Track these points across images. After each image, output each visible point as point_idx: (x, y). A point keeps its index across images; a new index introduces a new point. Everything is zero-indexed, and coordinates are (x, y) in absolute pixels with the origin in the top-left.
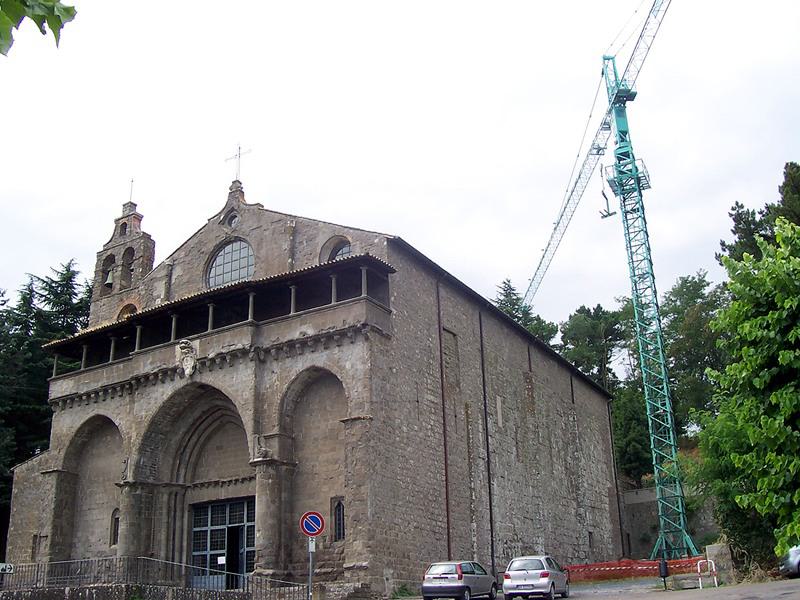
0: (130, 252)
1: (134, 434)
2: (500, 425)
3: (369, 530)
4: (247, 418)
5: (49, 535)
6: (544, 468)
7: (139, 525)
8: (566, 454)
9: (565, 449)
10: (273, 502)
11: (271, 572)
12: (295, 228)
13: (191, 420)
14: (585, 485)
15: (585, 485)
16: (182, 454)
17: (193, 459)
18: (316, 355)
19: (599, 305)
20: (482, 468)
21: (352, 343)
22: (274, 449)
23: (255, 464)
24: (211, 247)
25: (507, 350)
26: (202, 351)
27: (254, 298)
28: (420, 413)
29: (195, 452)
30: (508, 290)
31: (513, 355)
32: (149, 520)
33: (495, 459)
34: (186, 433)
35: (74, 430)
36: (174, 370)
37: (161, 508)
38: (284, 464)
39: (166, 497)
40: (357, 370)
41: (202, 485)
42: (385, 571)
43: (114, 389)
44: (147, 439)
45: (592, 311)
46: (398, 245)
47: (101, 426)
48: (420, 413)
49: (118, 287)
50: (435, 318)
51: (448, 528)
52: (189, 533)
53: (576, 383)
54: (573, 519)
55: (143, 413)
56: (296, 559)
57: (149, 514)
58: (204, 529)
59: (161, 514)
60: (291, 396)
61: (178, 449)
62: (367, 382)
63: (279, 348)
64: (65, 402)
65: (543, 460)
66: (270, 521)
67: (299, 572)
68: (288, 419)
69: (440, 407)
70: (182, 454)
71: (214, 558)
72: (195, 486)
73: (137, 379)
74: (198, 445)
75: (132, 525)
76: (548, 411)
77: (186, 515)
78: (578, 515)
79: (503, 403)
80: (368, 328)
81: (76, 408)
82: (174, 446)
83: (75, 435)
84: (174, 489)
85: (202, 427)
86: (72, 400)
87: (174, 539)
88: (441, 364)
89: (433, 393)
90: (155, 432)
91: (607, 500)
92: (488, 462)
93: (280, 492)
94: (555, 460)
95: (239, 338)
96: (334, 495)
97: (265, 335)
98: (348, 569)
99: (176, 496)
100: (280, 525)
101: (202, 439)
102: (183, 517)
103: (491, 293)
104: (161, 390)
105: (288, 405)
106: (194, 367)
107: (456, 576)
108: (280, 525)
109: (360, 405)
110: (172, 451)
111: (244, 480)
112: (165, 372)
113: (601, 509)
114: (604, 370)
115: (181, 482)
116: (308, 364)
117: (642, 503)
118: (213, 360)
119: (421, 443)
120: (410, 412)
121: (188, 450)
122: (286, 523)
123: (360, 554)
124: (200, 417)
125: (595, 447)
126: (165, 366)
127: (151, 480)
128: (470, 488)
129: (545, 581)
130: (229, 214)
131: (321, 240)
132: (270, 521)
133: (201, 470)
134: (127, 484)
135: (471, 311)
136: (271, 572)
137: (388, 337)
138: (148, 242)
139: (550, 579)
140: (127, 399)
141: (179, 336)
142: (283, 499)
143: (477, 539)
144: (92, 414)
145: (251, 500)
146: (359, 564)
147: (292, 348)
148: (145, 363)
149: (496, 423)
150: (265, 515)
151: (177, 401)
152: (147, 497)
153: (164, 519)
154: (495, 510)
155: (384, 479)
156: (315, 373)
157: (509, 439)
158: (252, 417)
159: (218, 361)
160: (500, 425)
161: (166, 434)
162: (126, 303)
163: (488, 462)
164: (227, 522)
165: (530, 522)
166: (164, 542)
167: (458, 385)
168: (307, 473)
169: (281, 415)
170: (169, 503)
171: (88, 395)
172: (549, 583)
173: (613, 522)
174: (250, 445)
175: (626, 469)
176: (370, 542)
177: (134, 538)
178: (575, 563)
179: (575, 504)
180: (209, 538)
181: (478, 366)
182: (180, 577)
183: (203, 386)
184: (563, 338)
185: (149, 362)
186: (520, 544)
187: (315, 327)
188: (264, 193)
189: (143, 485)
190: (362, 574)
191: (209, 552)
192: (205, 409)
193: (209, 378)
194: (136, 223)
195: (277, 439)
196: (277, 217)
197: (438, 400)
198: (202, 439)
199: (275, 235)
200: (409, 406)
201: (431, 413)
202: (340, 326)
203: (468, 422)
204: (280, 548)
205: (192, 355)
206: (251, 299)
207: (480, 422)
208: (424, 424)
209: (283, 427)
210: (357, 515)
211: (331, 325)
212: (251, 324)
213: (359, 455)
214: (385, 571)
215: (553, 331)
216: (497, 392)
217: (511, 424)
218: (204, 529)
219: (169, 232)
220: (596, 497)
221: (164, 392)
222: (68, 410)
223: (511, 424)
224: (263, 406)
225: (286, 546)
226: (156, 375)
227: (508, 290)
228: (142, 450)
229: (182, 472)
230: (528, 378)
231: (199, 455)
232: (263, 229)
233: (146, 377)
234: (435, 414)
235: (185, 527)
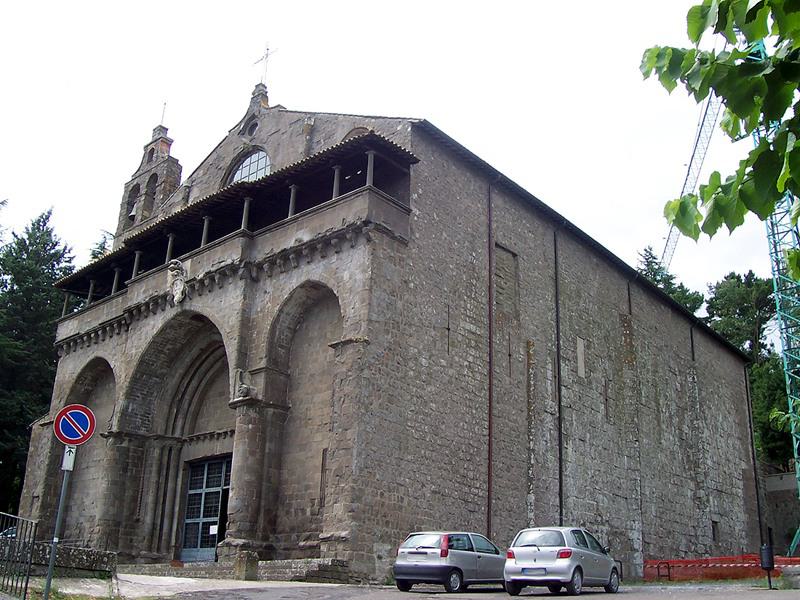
0: (154, 177)
2: (582, 372)
3: (353, 488)
5: (41, 495)
6: (647, 435)
7: (124, 483)
8: (681, 422)
9: (682, 410)
10: (252, 453)
11: (240, 541)
12: (312, 124)
13: (188, 360)
14: (709, 462)
15: (709, 462)
18: (313, 266)
19: (751, 271)
20: (550, 425)
21: (352, 247)
22: (259, 387)
23: (234, 406)
24: (228, 161)
25: (596, 285)
27: (250, 205)
28: (451, 344)
29: (195, 400)
30: (650, 259)
32: (136, 479)
33: (570, 417)
35: (75, 376)
36: (164, 297)
38: (270, 406)
39: (156, 452)
42: (376, 547)
43: (111, 325)
44: (135, 381)
45: (743, 278)
46: (424, 131)
47: (100, 371)
48: (451, 344)
49: (140, 218)
50: (483, 229)
51: (489, 497)
52: (183, 496)
53: (698, 337)
54: (689, 503)
55: (134, 351)
56: (280, 528)
57: (138, 472)
58: (199, 491)
59: (151, 472)
60: (286, 322)
61: (176, 394)
62: (366, 295)
63: (272, 261)
64: (68, 344)
65: (647, 423)
66: (247, 477)
67: (283, 544)
68: (282, 351)
69: (485, 341)
71: (207, 526)
73: (129, 311)
74: (199, 392)
76: (655, 365)
77: (181, 473)
78: (696, 498)
79: (588, 347)
80: (371, 226)
81: (80, 351)
82: (170, 392)
84: (169, 442)
86: (76, 343)
88: (490, 287)
89: (475, 321)
90: (145, 370)
91: (741, 484)
92: (560, 419)
93: (263, 440)
94: (664, 427)
95: (229, 252)
97: (259, 248)
98: (325, 540)
100: (260, 485)
102: (177, 476)
103: (635, 262)
104: (152, 323)
105: (282, 333)
107: (439, 551)
108: (260, 485)
109: (356, 326)
110: (168, 397)
113: (732, 494)
114: (757, 346)
115: (177, 434)
116: (303, 279)
117: (788, 491)
118: (201, 281)
119: (450, 382)
120: (434, 342)
121: (187, 397)
122: (269, 481)
123: (340, 521)
124: (199, 356)
125: (725, 417)
127: (142, 431)
128: (529, 449)
129: (564, 563)
130: (250, 124)
132: (247, 477)
133: (201, 421)
134: (111, 434)
135: (541, 230)
136: (240, 541)
137: (404, 243)
138: (174, 165)
139: (573, 560)
142: (267, 451)
143: (536, 516)
144: (92, 357)
145: (229, 456)
146: (337, 534)
147: (287, 260)
149: (575, 371)
150: (241, 468)
151: (170, 336)
152: (135, 451)
153: (154, 478)
154: (569, 482)
155: (386, 424)
156: (315, 292)
157: (595, 394)
158: (236, 347)
159: (206, 282)
160: (582, 372)
163: (560, 419)
164: (223, 484)
165: (623, 501)
166: (150, 506)
167: (517, 317)
168: (300, 418)
169: (272, 345)
171: (88, 334)
172: (570, 567)
173: (747, 511)
174: (231, 382)
175: (768, 449)
176: (355, 505)
177: (116, 498)
178: (691, 557)
179: (692, 485)
180: (203, 503)
181: (550, 296)
182: (168, 548)
183: (200, 318)
184: (708, 309)
186: (606, 528)
187: (312, 231)
190: (340, 547)
191: (202, 520)
192: (203, 347)
194: (165, 148)
195: (263, 375)
197: (484, 332)
199: (294, 139)
200: (433, 333)
201: (469, 346)
202: (338, 226)
203: (529, 364)
204: (257, 511)
205: (181, 277)
207: (550, 366)
208: (457, 359)
210: (340, 468)
212: (243, 234)
213: (347, 389)
214: (376, 547)
215: (697, 300)
216: (579, 334)
217: (598, 375)
218: (199, 491)
219: (190, 153)
220: (724, 479)
221: (154, 325)
222: (72, 354)
223: (598, 375)
224: (252, 334)
225: (268, 511)
227: (650, 259)
228: (130, 394)
229: (180, 423)
230: (626, 321)
232: (281, 132)
233: (138, 307)
234: (476, 348)
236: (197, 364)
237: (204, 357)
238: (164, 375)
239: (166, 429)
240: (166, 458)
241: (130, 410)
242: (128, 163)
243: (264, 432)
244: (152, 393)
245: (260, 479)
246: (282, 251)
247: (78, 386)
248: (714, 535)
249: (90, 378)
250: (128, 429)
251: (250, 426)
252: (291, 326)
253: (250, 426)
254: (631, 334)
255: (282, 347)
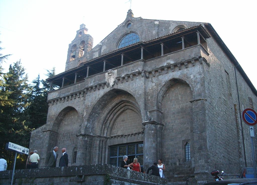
1: (85, 114)
4: (141, 104)
5: (45, 158)
7: (86, 154)
13: (110, 108)
16: (106, 123)
17: (111, 126)
26: (118, 74)
31: (142, 158)
32: (90, 152)
34: (108, 114)
35: (58, 113)
37: (96, 147)
40: (197, 78)
41: (115, 137)
47: (70, 110)
57: (91, 149)
58: (115, 157)
59: (96, 150)
68: (160, 104)
70: (106, 123)
72: (112, 137)
75: (83, 153)
83: (58, 116)
85: (115, 111)
87: (101, 161)
96: (184, 139)
98: (197, 174)
99: (103, 141)
101: (115, 116)
105: (160, 97)
106: (115, 82)
110: (101, 121)
111: (136, 134)
112: (100, 85)
115: (105, 135)
116: (171, 78)
118: (124, 78)
121: (109, 122)
124: (115, 106)
126: (100, 82)
127: (91, 134)
131: (175, 25)
133: (114, 131)
134: (81, 135)
140: (82, 99)
141: (107, 69)
142: (158, 141)
144: (66, 106)
148: (91, 82)
159: (126, 78)
161: (99, 114)
162: (81, 62)
170: (99, 145)
171: (64, 98)
185: (93, 81)
188: (141, 17)
189: (88, 136)
193: (121, 86)
195: (155, 112)
196: (150, 21)
198: (115, 116)
202: (187, 58)
206: (142, 50)
209: (158, 107)
211: (183, 59)
218: (115, 157)
221: (101, 92)
226: (96, 86)
229: (106, 131)
231: (113, 125)
233: (92, 88)
235: (107, 156)
236: (114, 109)
237: (117, 107)
238: (100, 113)
239: (101, 134)
240: (101, 144)
241: (88, 126)
242: (71, 37)
243: (157, 134)
244: (95, 120)
245: (157, 151)
246: (161, 67)
247: (58, 117)
248: (43, 177)
249: (63, 114)
250: (87, 133)
251: (153, 132)
252: (163, 95)
253: (153, 132)
254: (253, 104)
255: (160, 102)
